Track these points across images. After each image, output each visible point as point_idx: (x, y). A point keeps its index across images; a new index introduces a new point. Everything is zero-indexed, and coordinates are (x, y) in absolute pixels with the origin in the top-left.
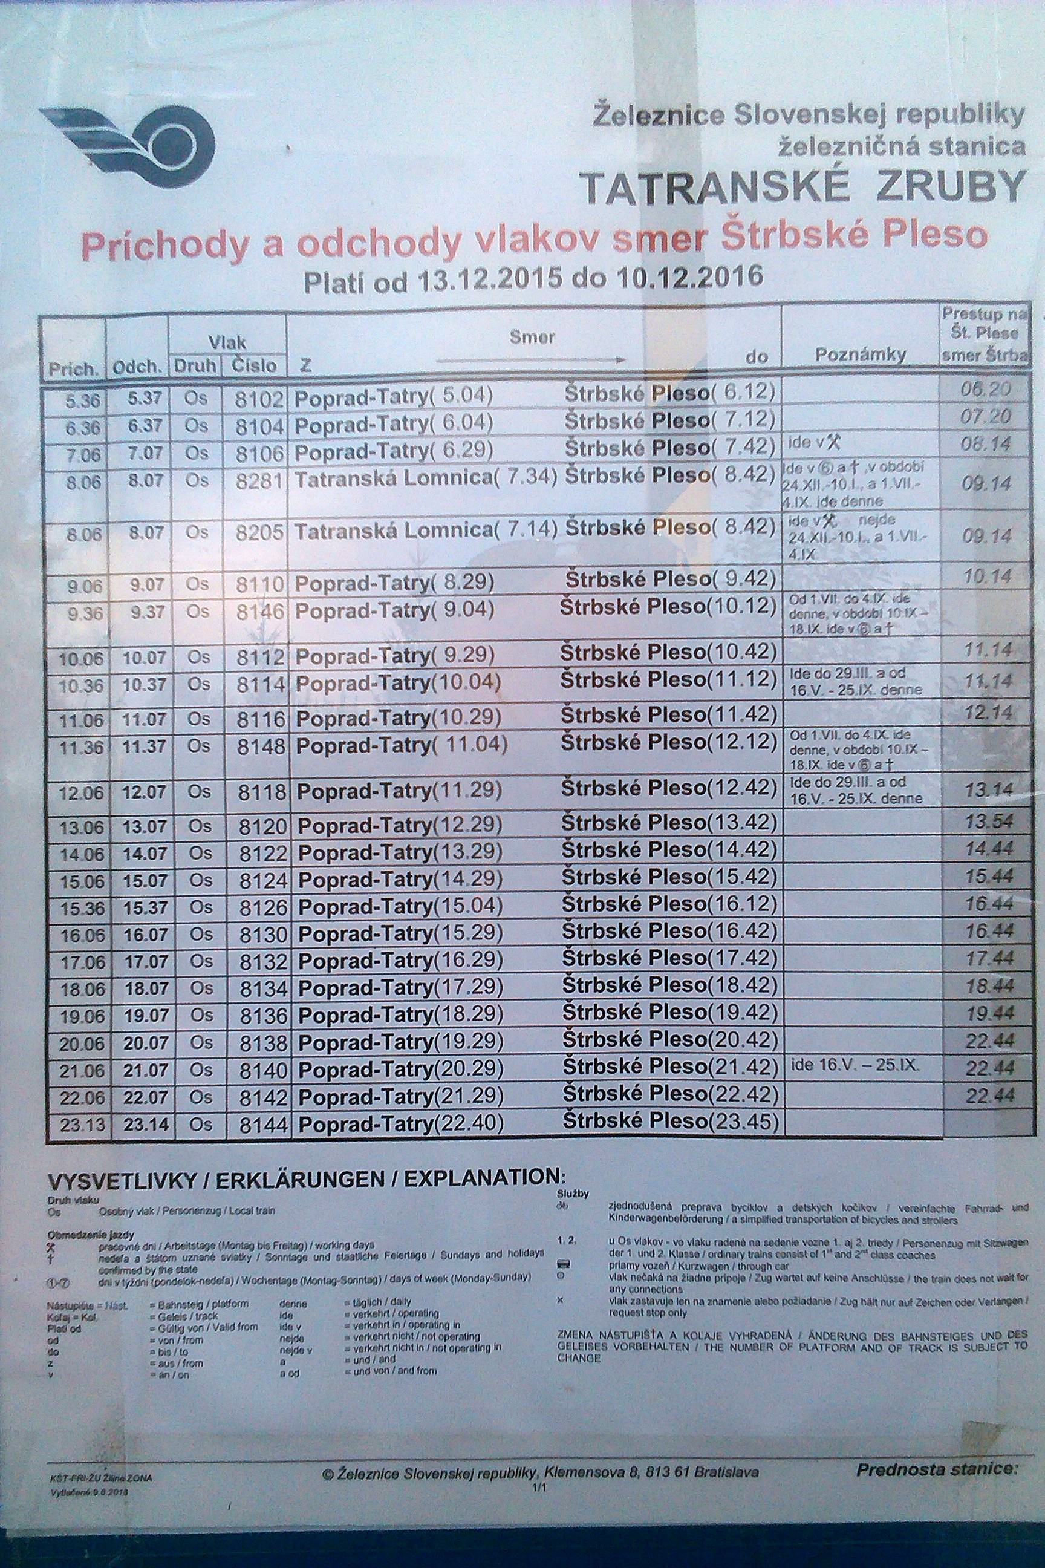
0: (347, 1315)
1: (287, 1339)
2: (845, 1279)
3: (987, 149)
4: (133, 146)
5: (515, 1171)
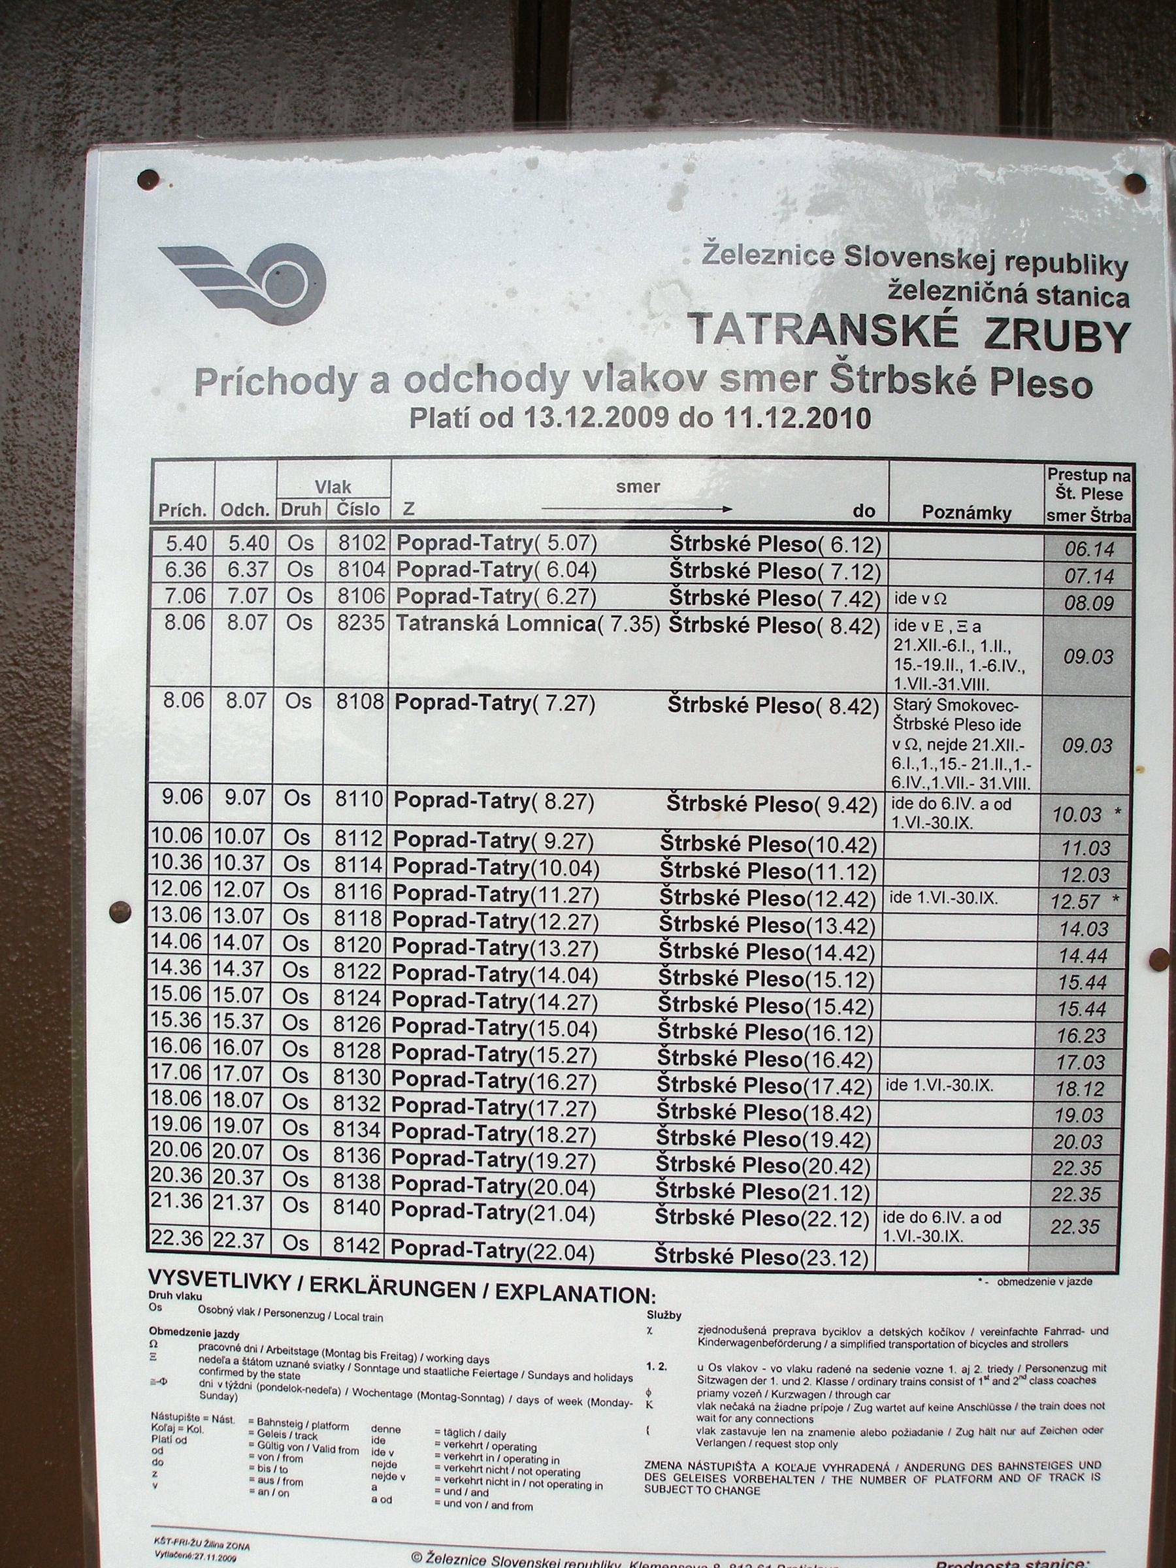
2: (951, 1408)
5: (605, 1289)
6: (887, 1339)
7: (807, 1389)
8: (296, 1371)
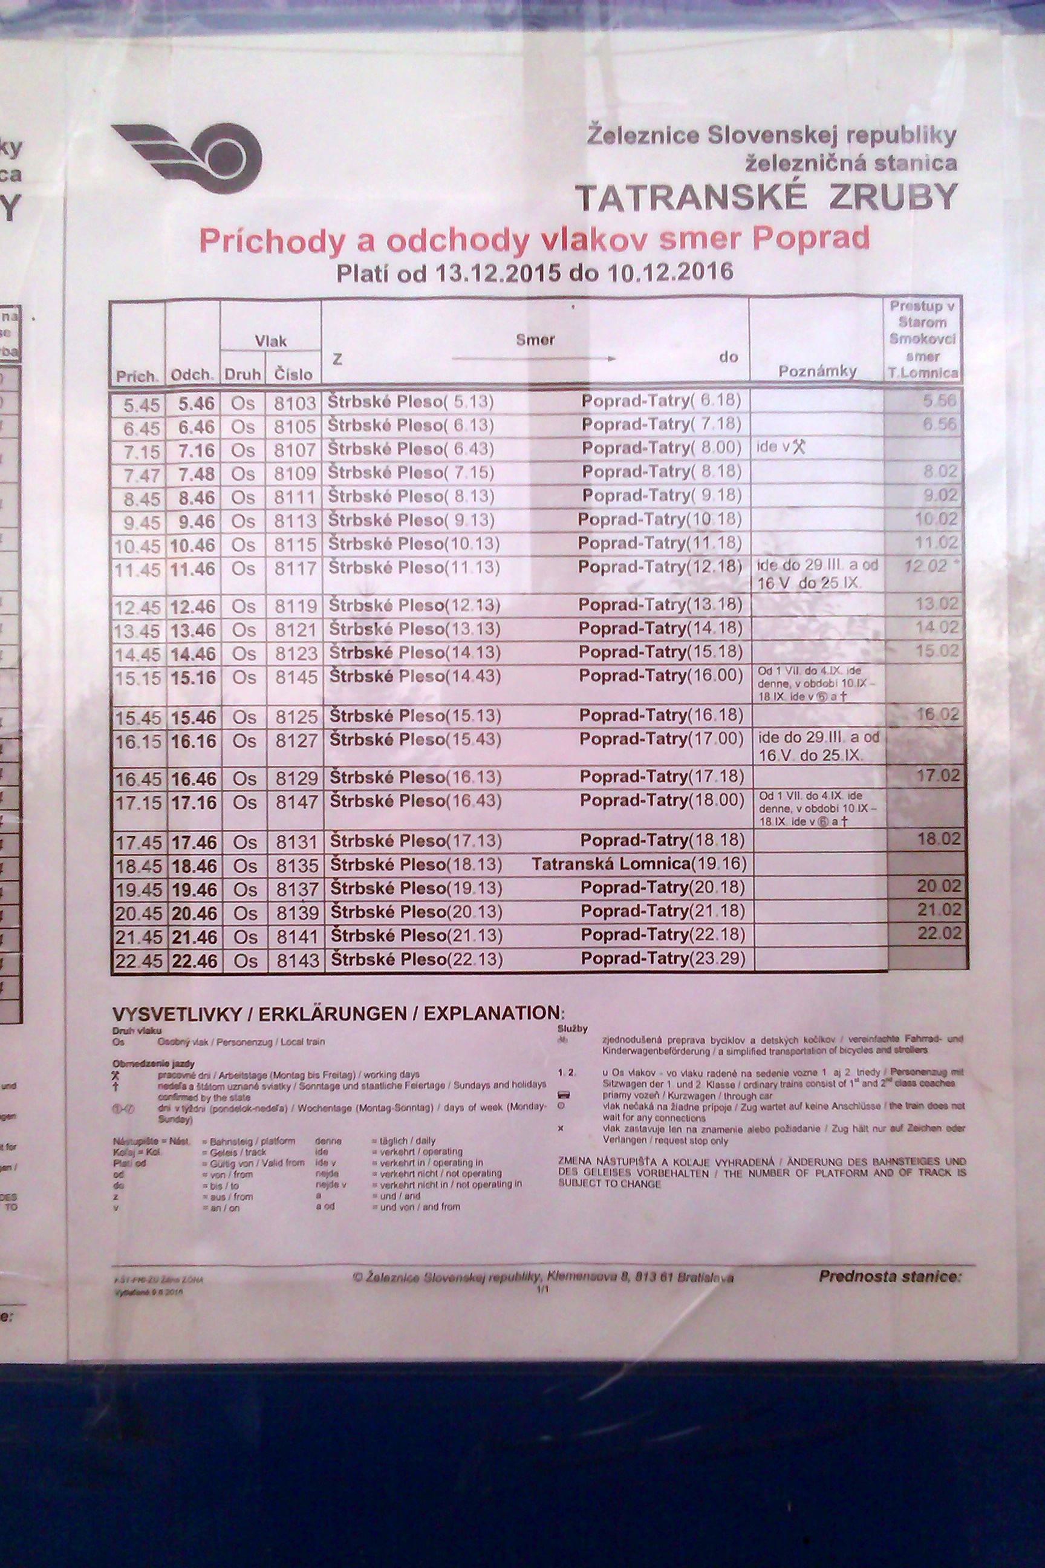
0: (375, 1174)
1: (323, 1174)
2: (826, 1107)
3: (819, 164)
4: (190, 157)
5: (521, 1008)
6: (768, 1046)
7: (699, 1092)
8: (247, 1092)
